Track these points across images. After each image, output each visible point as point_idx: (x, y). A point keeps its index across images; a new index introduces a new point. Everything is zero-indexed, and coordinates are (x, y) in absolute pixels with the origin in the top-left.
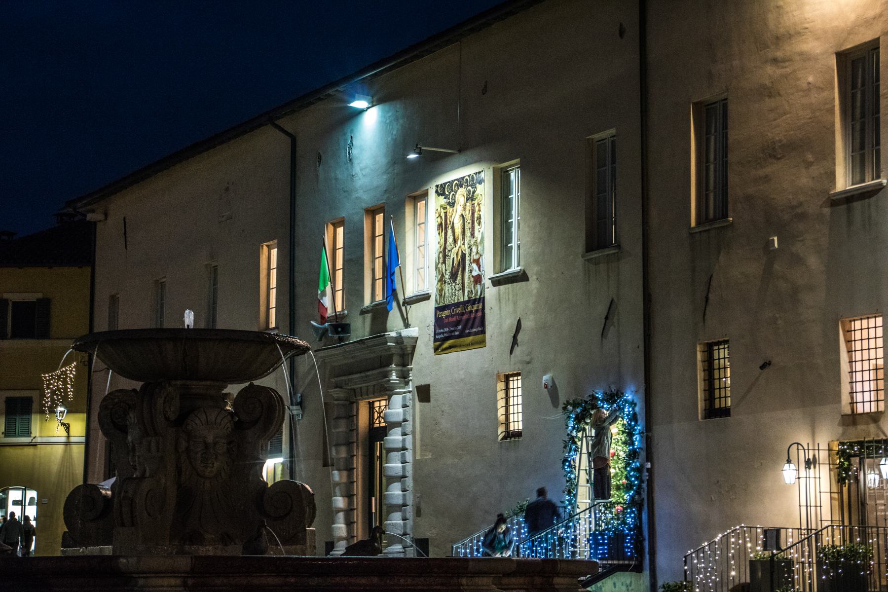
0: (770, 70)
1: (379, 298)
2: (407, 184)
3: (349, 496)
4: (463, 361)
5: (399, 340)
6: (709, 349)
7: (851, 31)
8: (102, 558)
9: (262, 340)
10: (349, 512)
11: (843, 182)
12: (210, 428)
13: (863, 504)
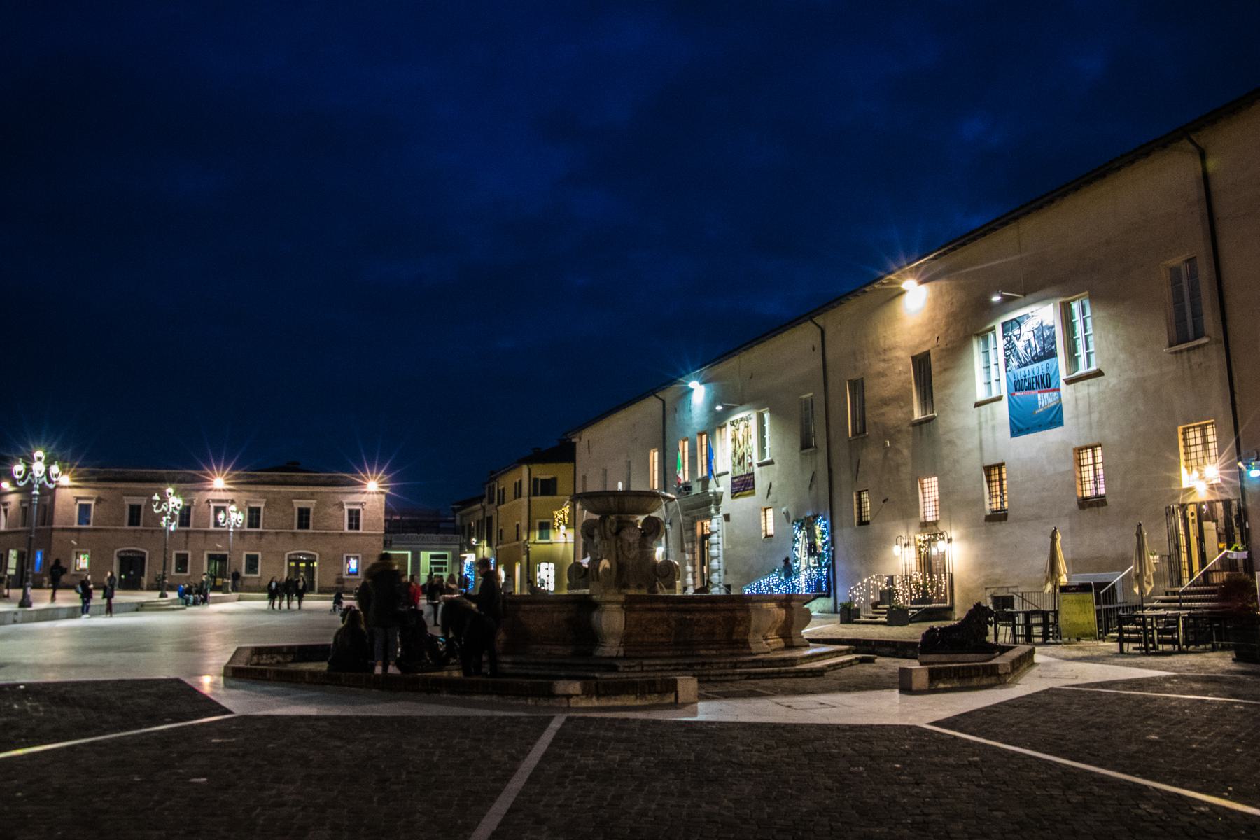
0: (882, 364)
1: (705, 474)
2: (716, 422)
3: (694, 565)
4: (745, 502)
5: (715, 493)
6: (859, 494)
7: (918, 347)
8: (585, 596)
9: (653, 496)
10: (694, 573)
11: (917, 416)
12: (631, 537)
13: (930, 563)
